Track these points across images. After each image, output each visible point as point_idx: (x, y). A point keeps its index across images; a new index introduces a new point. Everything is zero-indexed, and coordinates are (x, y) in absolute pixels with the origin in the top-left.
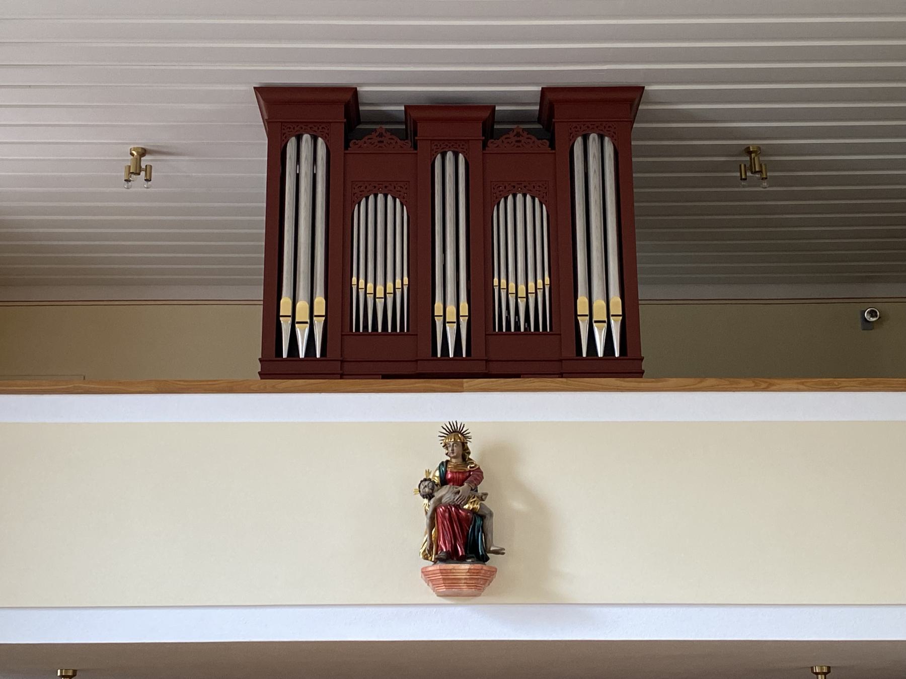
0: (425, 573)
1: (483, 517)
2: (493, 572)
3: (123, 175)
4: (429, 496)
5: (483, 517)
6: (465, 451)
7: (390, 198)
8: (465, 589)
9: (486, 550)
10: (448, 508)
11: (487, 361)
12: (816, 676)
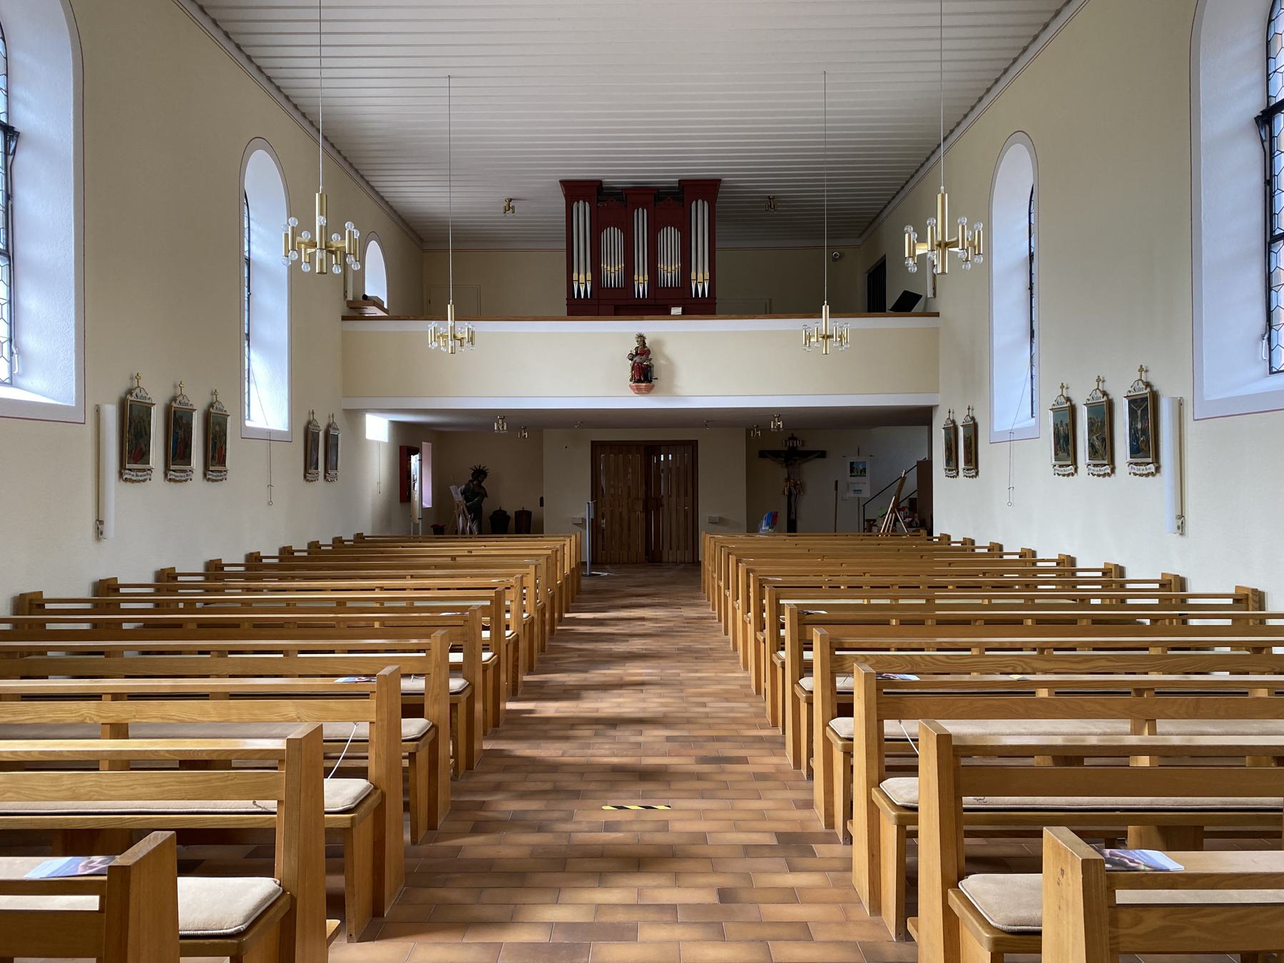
0: (630, 386)
1: (650, 367)
2: (653, 386)
3: (503, 211)
4: (632, 360)
5: (650, 367)
6: (644, 343)
7: (616, 229)
8: (644, 392)
9: (651, 378)
10: (638, 363)
11: (655, 299)
12: (782, 473)
